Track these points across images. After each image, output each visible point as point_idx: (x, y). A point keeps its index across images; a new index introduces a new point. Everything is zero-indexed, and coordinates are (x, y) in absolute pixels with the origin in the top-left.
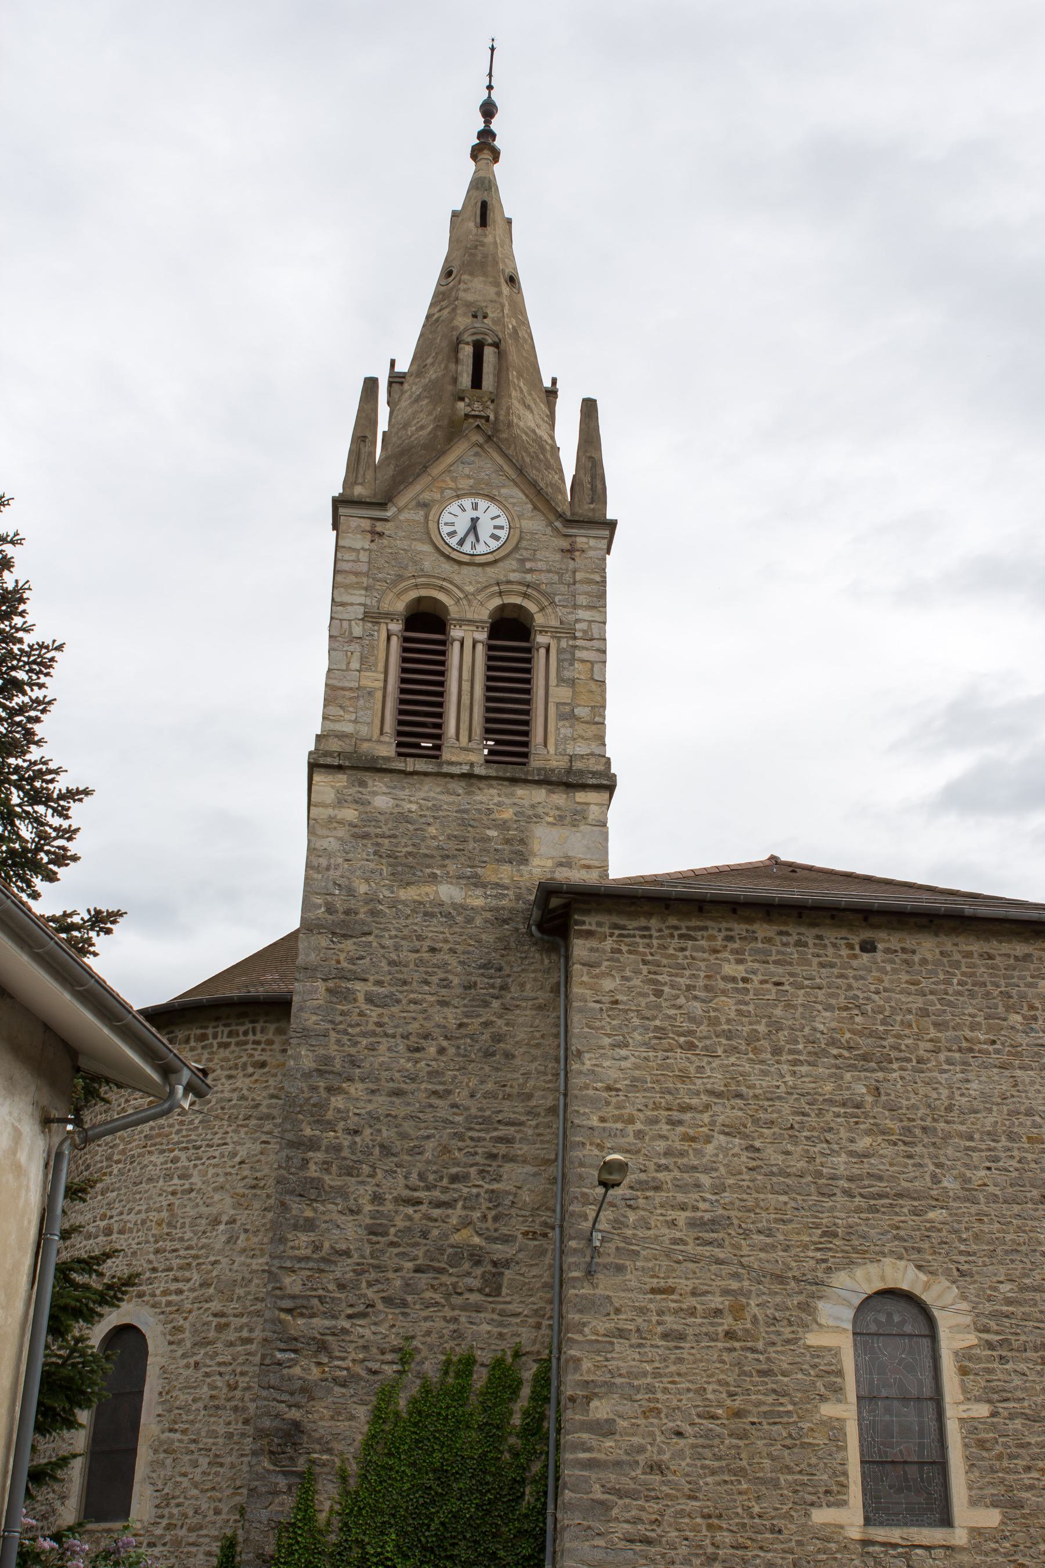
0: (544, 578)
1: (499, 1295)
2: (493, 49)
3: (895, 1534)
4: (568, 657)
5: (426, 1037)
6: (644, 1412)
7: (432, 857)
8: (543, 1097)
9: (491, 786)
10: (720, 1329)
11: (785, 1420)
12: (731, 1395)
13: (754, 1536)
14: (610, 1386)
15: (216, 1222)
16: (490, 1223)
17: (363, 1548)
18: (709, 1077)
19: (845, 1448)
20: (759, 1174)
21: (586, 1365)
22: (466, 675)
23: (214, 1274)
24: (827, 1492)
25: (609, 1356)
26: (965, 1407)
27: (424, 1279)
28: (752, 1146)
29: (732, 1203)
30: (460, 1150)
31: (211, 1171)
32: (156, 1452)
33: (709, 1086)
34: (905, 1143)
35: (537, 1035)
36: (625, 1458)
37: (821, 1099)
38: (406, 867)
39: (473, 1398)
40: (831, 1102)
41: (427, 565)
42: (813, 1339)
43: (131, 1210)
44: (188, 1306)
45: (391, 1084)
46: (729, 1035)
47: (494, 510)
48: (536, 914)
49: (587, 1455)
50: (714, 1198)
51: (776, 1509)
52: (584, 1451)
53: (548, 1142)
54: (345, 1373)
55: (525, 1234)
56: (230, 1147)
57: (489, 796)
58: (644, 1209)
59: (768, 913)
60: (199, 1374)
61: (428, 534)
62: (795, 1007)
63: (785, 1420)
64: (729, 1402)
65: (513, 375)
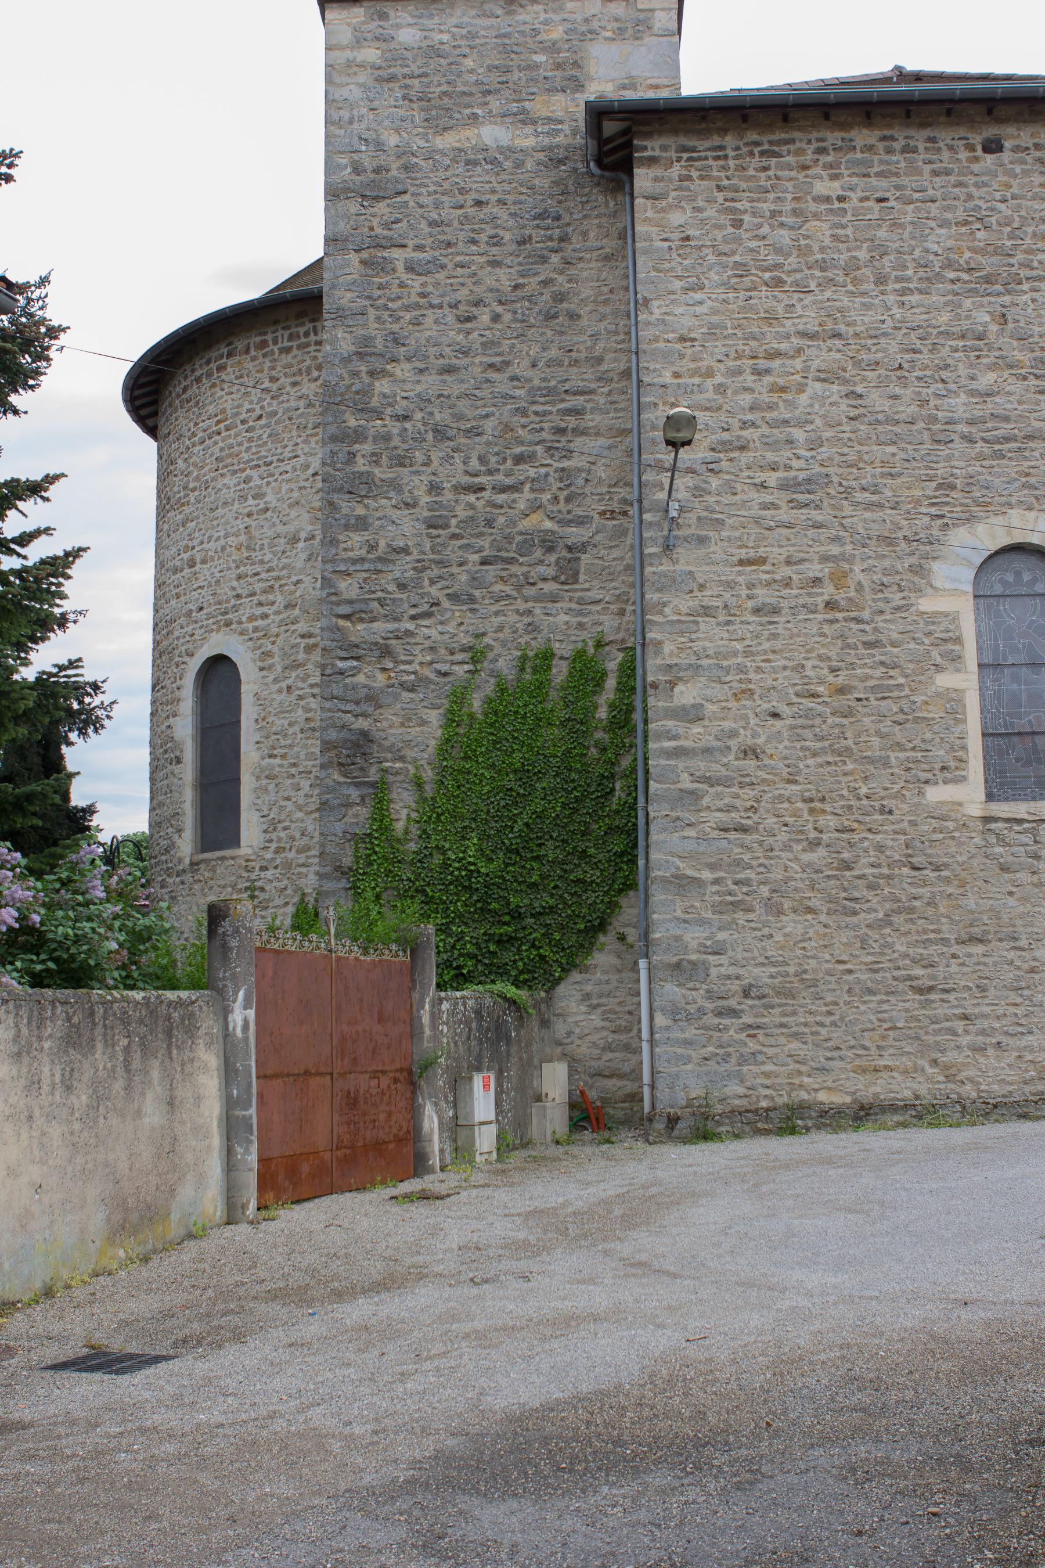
1: (576, 582)
3: (1020, 809)
5: (477, 304)
6: (735, 695)
7: (471, 94)
8: (615, 360)
10: (819, 599)
11: (895, 694)
12: (834, 670)
13: (861, 818)
14: (696, 668)
15: (295, 540)
16: (562, 506)
17: (444, 854)
18: (801, 316)
19: (964, 721)
20: (862, 423)
21: (668, 648)
23: (298, 594)
24: (943, 768)
25: (693, 636)
27: (491, 572)
28: (853, 392)
29: (831, 459)
30: (524, 427)
31: (285, 487)
32: (258, 778)
33: (801, 327)
34: (1037, 377)
35: (605, 289)
36: (715, 744)
37: (935, 332)
38: (441, 109)
39: (553, 694)
40: (947, 334)
42: (926, 604)
43: (210, 538)
44: (274, 630)
45: (442, 361)
46: (823, 266)
48: (592, 145)
49: (673, 744)
50: (809, 454)
51: (887, 789)
52: (670, 739)
53: (624, 410)
54: (413, 677)
55: (602, 513)
56: (302, 460)
58: (728, 473)
59: (868, 116)
60: (293, 698)
62: (902, 226)
63: (895, 694)
64: (831, 678)
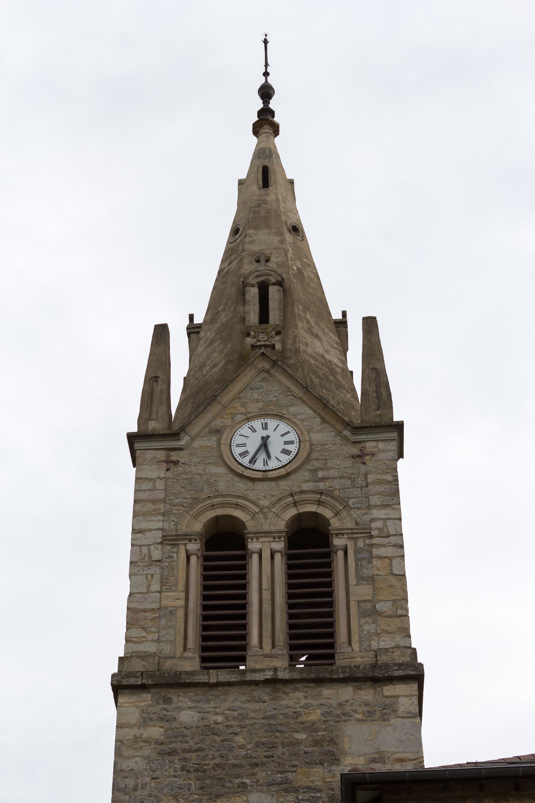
0: (336, 484)
2: (266, 42)
4: (367, 556)
7: (241, 766)
9: (296, 689)
22: (266, 585)
41: (222, 486)
47: (284, 427)
57: (295, 699)
61: (221, 457)
65: (299, 309)
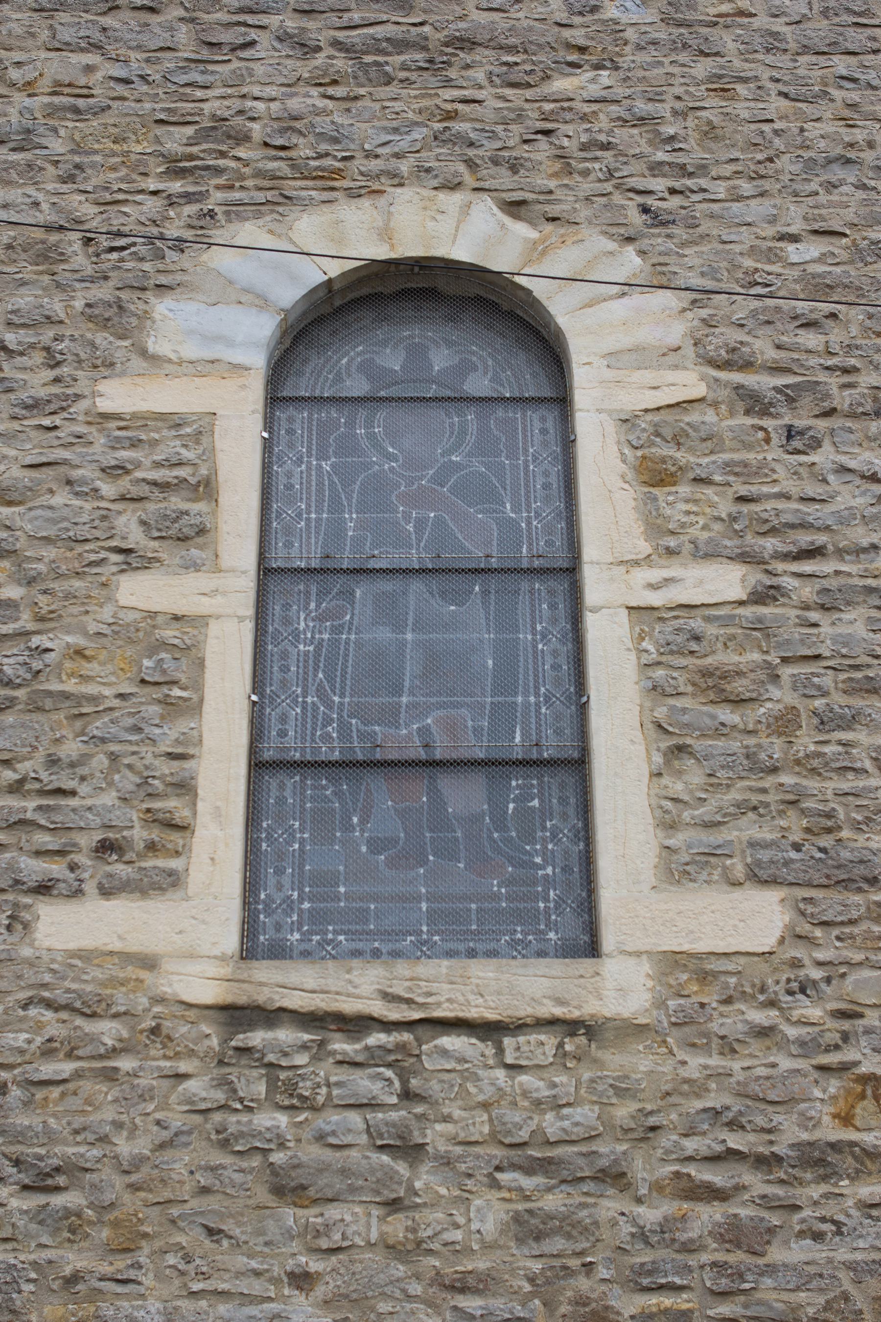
19: (195, 708)
26: (655, 575)
